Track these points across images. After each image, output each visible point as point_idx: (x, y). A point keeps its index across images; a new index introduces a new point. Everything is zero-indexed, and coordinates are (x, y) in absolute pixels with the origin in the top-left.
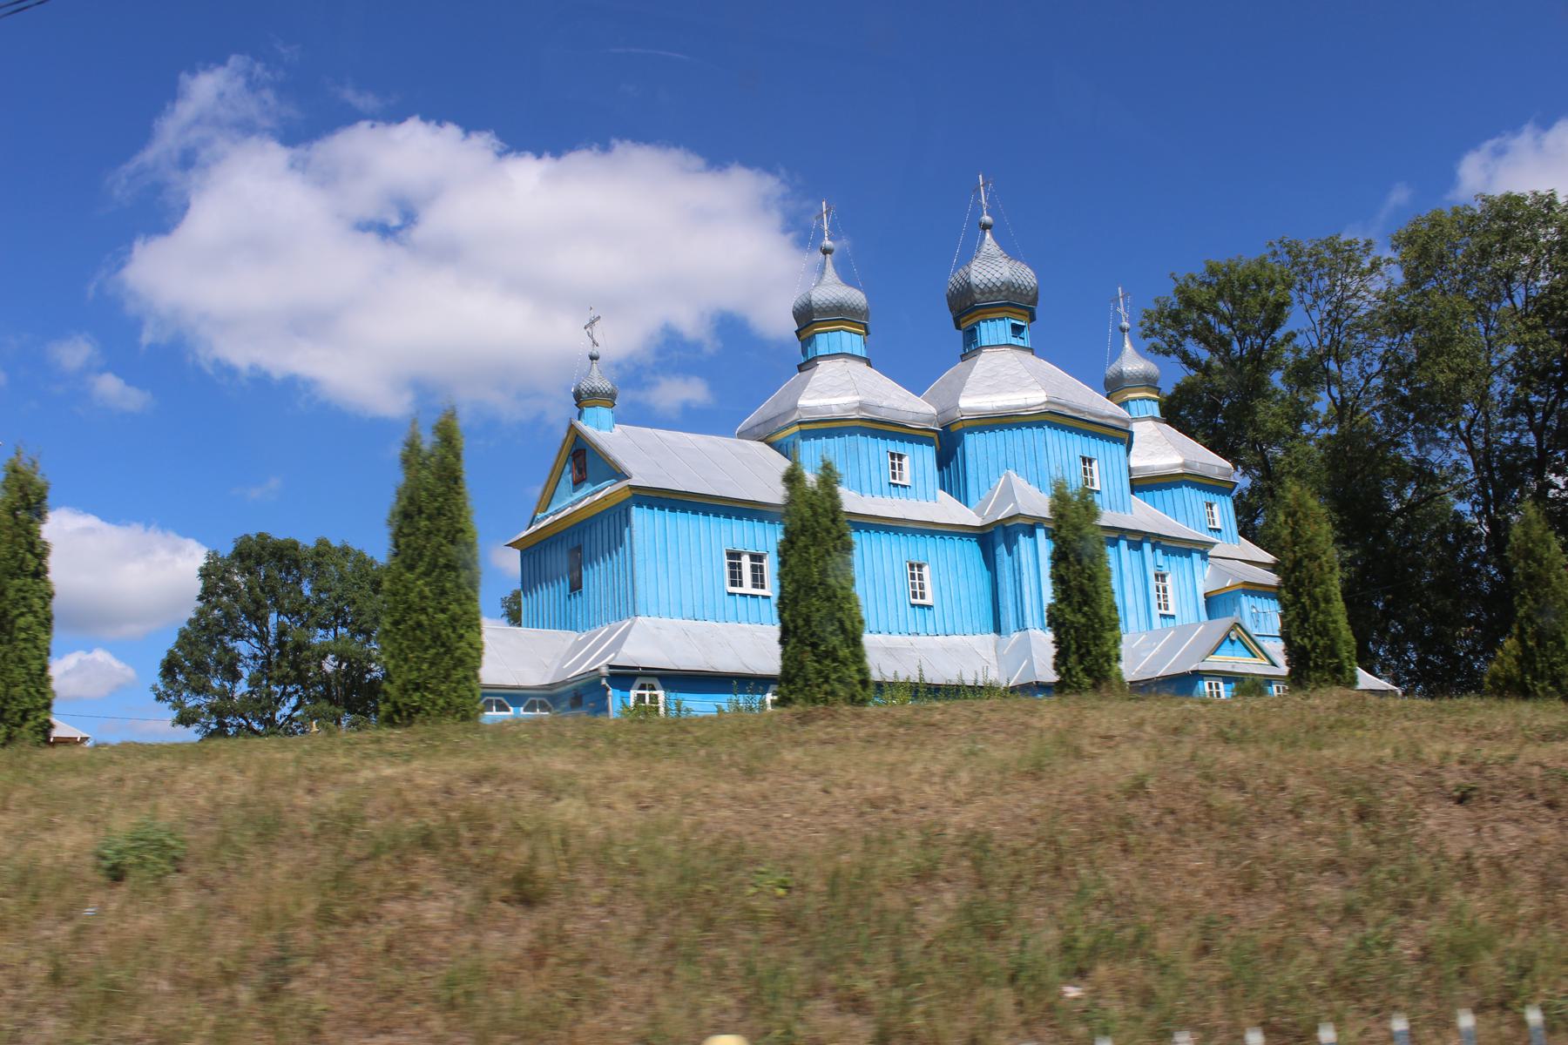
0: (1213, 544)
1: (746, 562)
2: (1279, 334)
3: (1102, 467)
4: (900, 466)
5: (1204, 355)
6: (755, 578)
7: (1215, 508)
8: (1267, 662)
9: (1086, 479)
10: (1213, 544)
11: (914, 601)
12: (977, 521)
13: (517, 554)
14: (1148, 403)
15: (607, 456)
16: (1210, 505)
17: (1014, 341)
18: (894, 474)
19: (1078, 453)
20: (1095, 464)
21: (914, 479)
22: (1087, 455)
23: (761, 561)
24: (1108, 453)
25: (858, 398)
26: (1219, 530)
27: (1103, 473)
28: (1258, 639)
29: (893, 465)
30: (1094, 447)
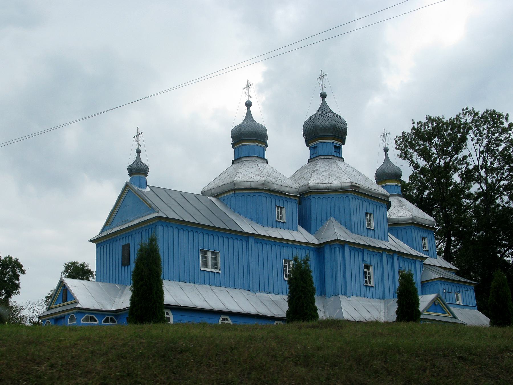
0: (426, 258)
1: (209, 255)
2: (460, 155)
3: (375, 218)
4: (281, 213)
5: (422, 163)
6: (213, 264)
7: (426, 240)
8: (451, 316)
9: (368, 224)
10: (426, 258)
11: (365, 284)
12: (316, 242)
13: (94, 245)
14: (396, 187)
15: (345, 256)
16: (424, 238)
17: (335, 154)
18: (278, 217)
19: (365, 211)
20: (372, 216)
21: (288, 219)
22: (368, 212)
23: (216, 255)
24: (378, 211)
25: (263, 179)
26: (428, 251)
27: (376, 220)
28: (449, 305)
29: (278, 212)
30: (371, 208)
